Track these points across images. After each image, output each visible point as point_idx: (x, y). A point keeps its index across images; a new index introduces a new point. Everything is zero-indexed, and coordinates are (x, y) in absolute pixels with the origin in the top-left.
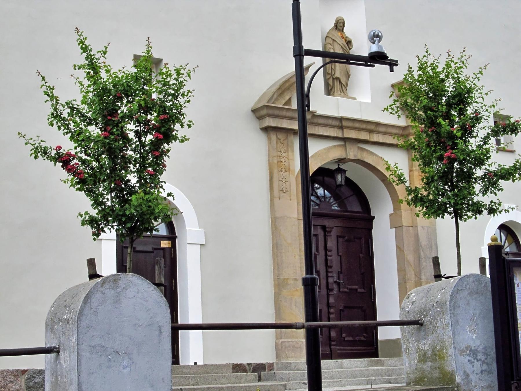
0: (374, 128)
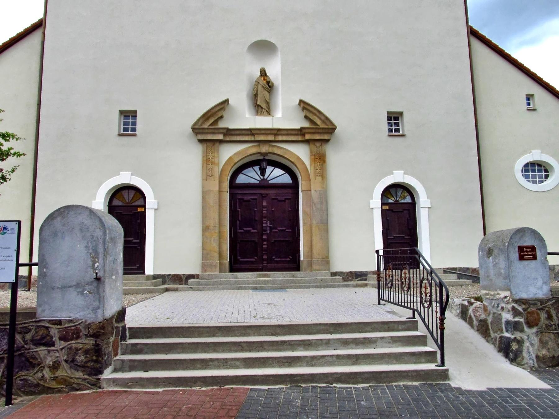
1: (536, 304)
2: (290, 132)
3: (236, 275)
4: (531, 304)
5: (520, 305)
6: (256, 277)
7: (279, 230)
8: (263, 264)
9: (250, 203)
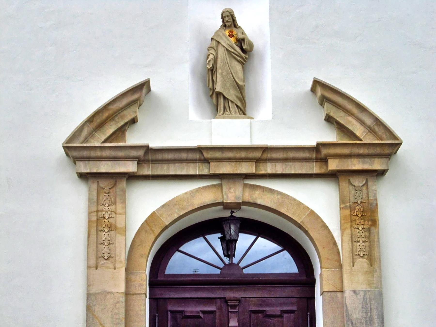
0: (260, 155)
2: (291, 155)
9: (200, 320)
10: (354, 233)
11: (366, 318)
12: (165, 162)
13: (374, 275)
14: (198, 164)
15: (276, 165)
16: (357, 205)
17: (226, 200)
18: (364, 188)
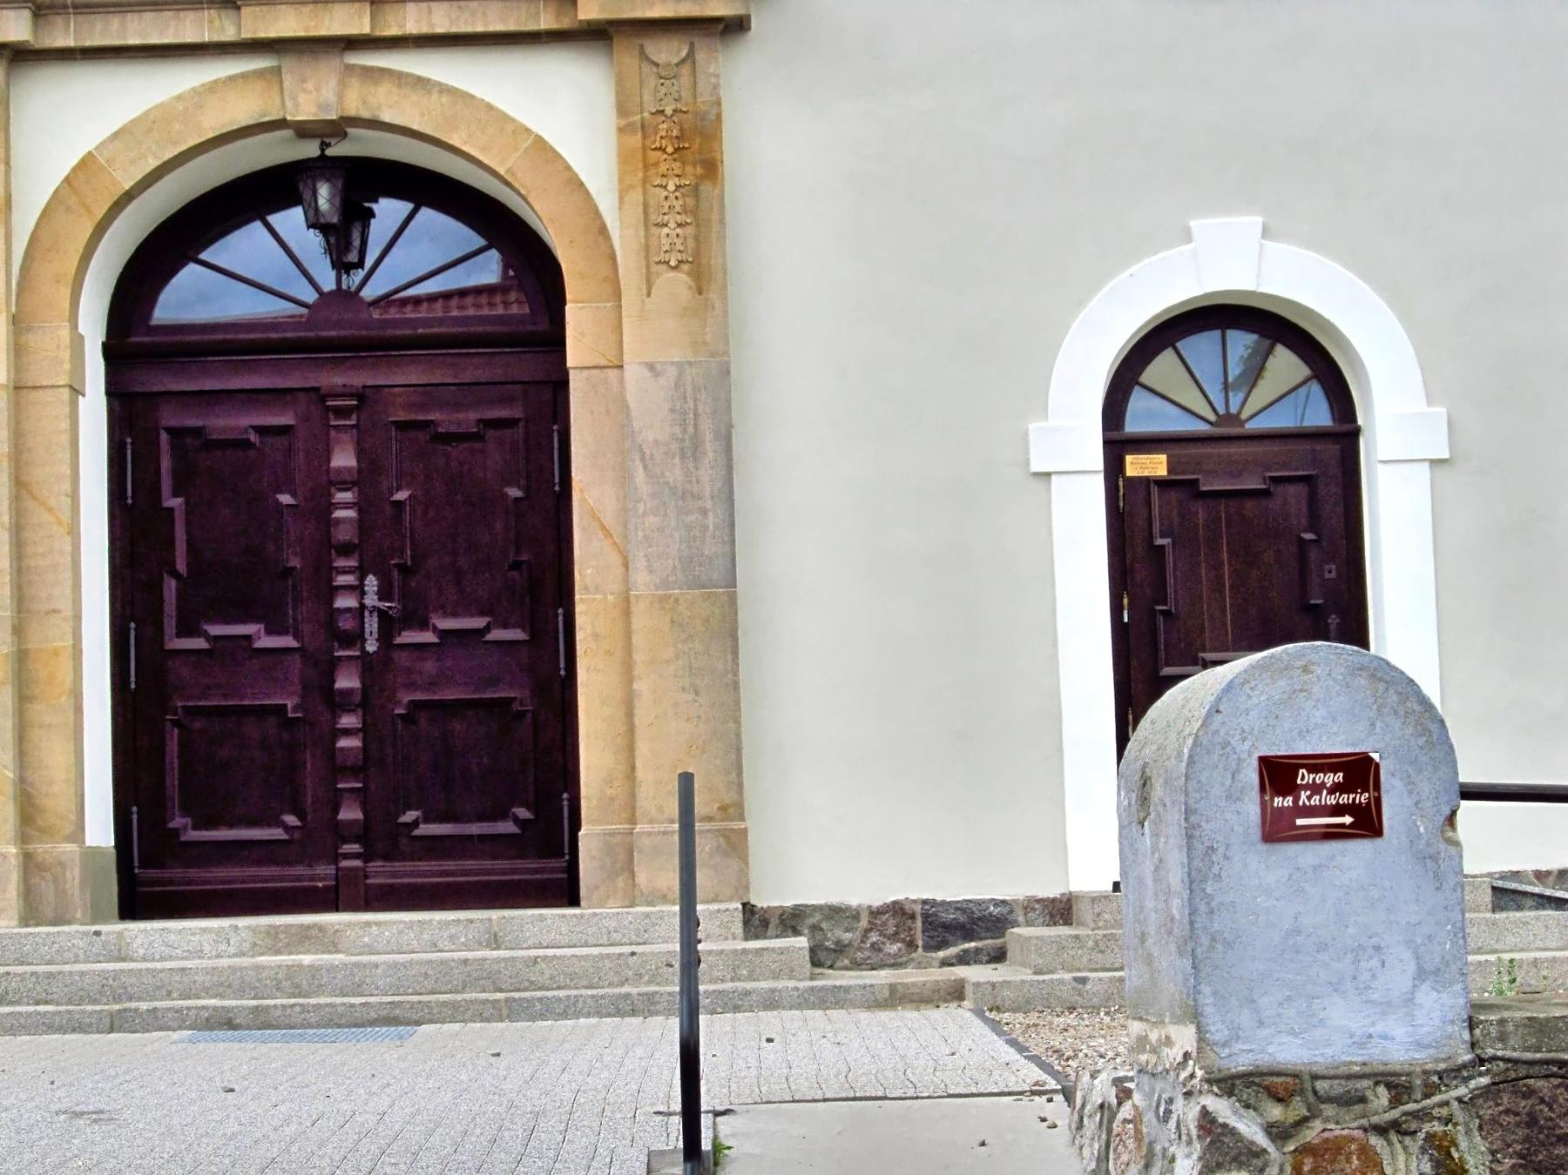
1: (1363, 1100)
3: (120, 934)
4: (1330, 1100)
5: (1247, 1106)
6: (245, 948)
7: (444, 634)
8: (336, 862)
9: (252, 453)
10: (652, 202)
11: (683, 440)
12: (112, 9)
13: (705, 320)
14: (210, 14)
15: (429, 7)
16: (663, 118)
17: (291, 114)
18: (685, 70)
